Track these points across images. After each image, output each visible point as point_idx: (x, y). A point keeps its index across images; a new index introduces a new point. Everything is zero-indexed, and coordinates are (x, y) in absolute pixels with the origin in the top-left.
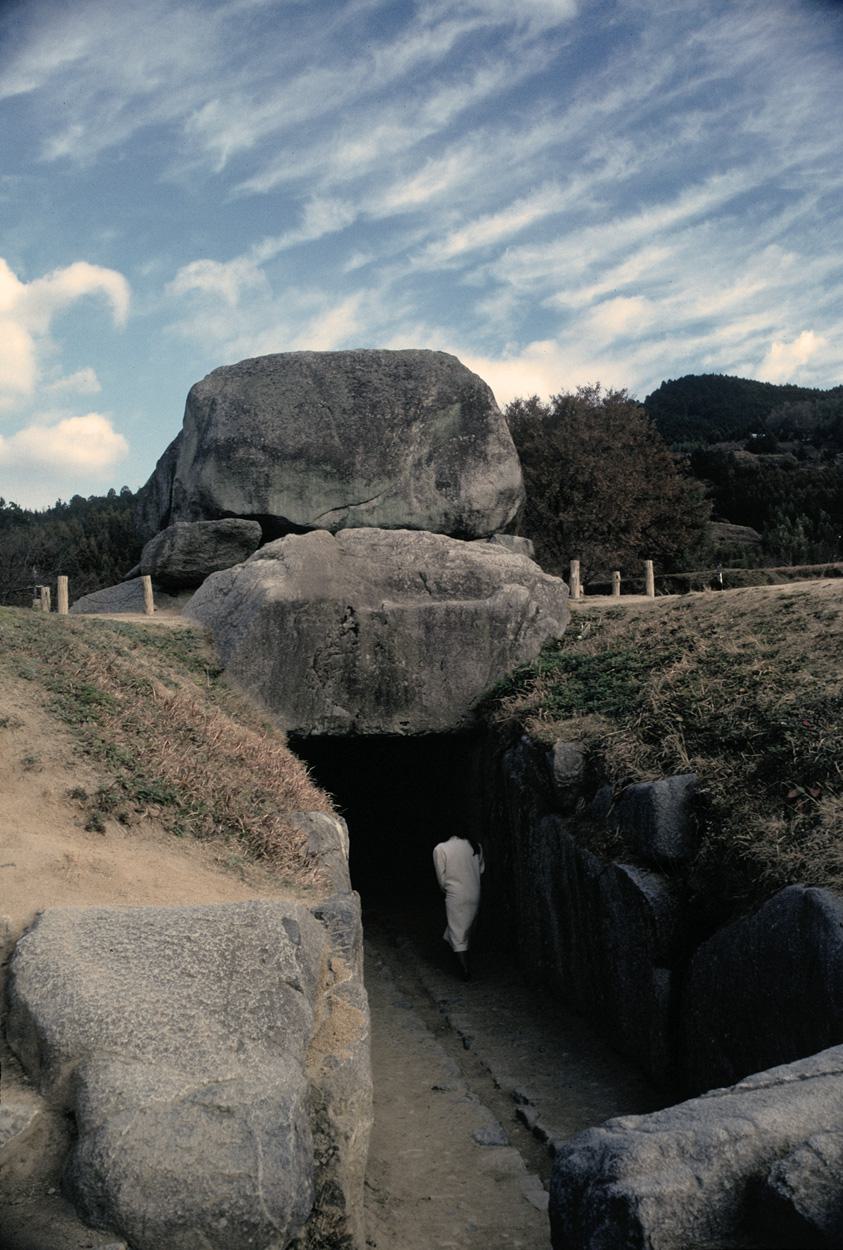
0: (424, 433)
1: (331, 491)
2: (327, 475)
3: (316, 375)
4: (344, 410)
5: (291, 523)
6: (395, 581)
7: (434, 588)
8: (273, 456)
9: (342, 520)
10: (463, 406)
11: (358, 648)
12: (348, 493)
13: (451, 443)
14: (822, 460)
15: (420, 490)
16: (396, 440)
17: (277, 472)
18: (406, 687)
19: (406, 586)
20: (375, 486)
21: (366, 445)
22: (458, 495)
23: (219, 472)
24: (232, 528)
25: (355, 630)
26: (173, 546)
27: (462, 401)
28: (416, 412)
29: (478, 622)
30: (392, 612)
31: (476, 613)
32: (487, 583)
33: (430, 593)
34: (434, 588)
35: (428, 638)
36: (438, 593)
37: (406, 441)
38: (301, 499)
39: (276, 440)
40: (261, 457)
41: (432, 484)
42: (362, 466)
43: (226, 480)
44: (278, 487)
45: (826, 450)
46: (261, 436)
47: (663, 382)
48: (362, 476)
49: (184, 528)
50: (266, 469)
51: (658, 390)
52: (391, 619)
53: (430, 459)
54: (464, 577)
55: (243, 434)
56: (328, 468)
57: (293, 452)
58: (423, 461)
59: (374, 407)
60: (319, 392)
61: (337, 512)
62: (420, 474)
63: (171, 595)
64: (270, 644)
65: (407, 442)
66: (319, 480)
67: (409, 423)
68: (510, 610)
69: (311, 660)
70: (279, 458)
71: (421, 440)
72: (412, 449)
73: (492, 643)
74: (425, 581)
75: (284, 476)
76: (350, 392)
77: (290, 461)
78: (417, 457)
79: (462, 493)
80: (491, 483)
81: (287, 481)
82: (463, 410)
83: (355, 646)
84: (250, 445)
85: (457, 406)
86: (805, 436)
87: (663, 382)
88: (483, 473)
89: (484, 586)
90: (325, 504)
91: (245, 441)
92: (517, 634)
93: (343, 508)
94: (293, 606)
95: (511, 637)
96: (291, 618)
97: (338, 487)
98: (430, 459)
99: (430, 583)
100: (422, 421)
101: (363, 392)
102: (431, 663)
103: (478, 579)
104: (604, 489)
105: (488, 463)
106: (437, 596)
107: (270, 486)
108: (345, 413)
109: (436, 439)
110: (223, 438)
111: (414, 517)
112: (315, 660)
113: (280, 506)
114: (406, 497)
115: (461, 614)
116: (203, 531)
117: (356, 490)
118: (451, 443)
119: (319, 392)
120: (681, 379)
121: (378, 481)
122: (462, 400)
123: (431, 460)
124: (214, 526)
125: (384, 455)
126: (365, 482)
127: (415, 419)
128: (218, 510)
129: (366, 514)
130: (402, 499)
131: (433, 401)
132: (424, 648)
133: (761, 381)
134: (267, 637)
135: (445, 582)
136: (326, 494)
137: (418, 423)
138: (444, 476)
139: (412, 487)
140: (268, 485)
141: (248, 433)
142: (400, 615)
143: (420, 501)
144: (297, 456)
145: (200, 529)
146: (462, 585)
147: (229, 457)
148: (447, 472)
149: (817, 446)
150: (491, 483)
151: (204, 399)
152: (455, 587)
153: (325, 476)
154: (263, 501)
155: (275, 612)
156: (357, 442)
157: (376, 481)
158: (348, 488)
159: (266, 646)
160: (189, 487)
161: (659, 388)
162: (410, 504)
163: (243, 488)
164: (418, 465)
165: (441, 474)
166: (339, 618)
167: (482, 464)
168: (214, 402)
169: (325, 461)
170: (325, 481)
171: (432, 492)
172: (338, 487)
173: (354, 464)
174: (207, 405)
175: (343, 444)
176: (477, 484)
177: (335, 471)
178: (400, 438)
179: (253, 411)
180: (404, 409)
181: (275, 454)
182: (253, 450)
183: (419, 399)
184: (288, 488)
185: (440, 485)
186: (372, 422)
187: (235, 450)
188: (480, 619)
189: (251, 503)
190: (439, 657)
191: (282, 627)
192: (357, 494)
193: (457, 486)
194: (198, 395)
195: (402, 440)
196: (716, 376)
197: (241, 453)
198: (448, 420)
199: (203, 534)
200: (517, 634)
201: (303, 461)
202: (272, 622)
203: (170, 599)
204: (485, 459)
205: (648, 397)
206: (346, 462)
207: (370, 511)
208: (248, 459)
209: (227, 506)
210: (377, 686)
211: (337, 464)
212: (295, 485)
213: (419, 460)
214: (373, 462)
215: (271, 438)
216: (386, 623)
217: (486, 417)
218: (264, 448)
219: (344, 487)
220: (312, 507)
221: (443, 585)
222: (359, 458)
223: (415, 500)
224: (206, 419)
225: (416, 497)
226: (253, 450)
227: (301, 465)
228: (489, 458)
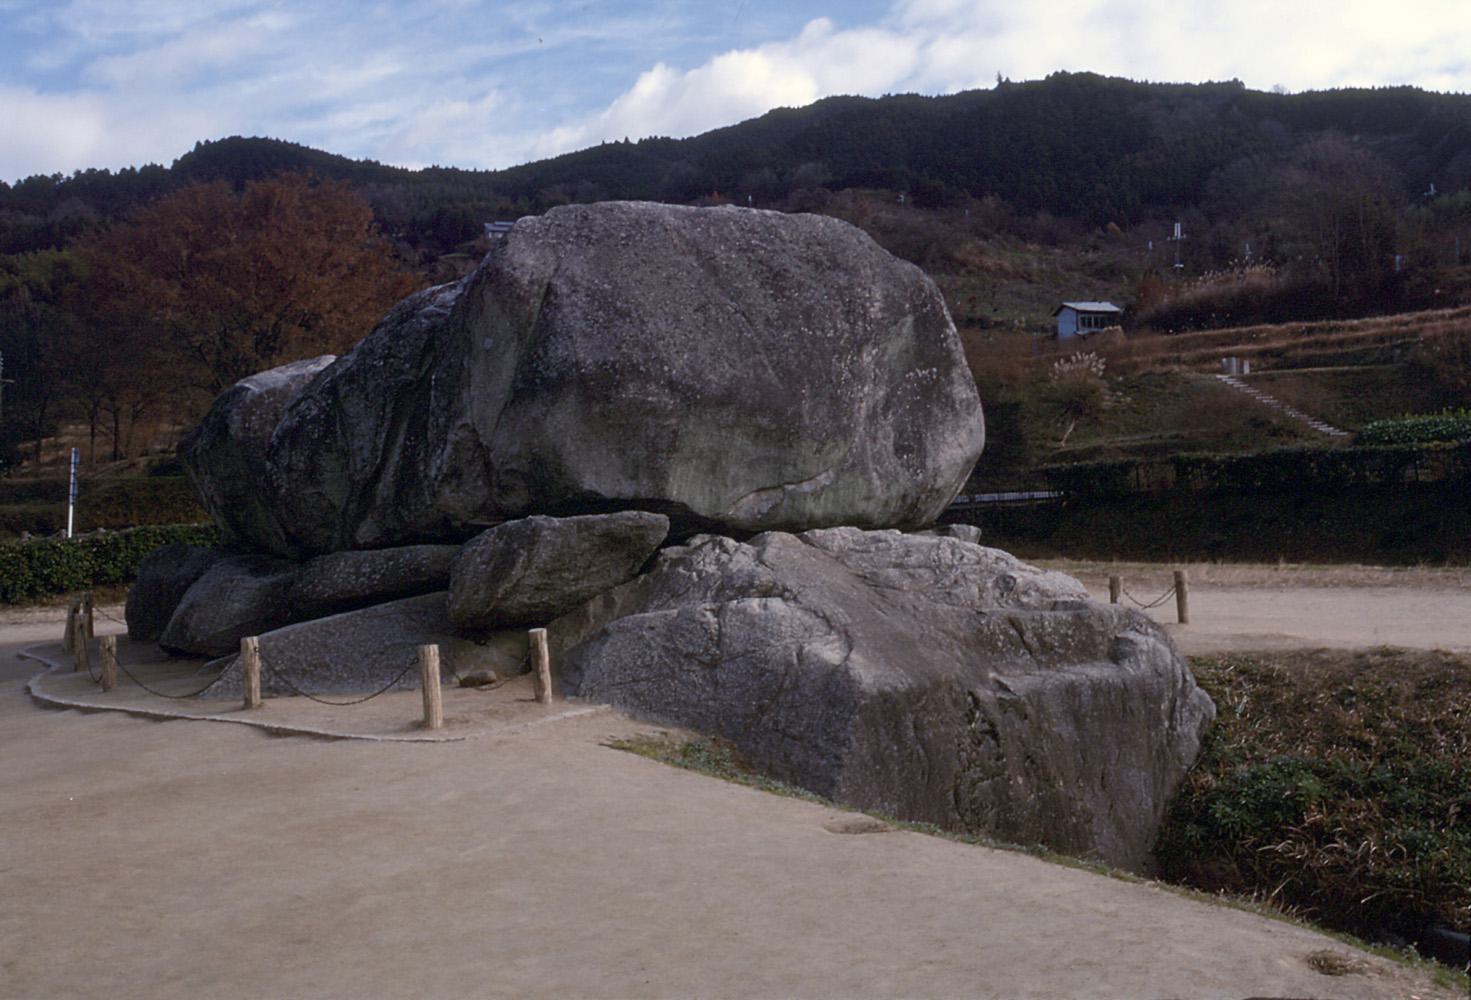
0: (878, 363)
2: (760, 434)
3: (699, 252)
4: (768, 319)
7: (1034, 643)
8: (688, 398)
10: (915, 320)
11: (1005, 767)
12: (786, 464)
13: (908, 381)
14: (421, 263)
15: (878, 459)
16: (846, 374)
19: (1000, 644)
20: (829, 453)
21: (811, 383)
22: (923, 466)
24: (631, 528)
30: (586, 612)
31: (1126, 689)
33: (1031, 653)
34: (1034, 643)
36: (1043, 653)
37: (858, 377)
39: (687, 370)
40: (668, 401)
41: (890, 445)
42: (811, 419)
45: (426, 250)
46: (663, 363)
47: (198, 144)
48: (812, 436)
49: (554, 529)
50: (673, 421)
51: (190, 153)
54: (1071, 624)
56: (765, 422)
58: (879, 410)
59: (808, 314)
61: (764, 496)
62: (876, 431)
63: (478, 643)
65: (860, 379)
66: (746, 442)
67: (858, 346)
68: (1161, 680)
69: (951, 795)
70: (697, 403)
71: (876, 375)
72: (866, 389)
73: (1149, 736)
74: (1021, 633)
76: (762, 285)
78: (871, 404)
79: (929, 463)
81: (702, 442)
82: (917, 323)
83: (1000, 763)
84: (647, 377)
85: (910, 319)
86: (396, 229)
87: (198, 144)
88: (954, 431)
89: (1099, 639)
91: (635, 367)
92: (1171, 718)
95: (1167, 724)
97: (774, 452)
98: (887, 407)
99: (1029, 636)
100: (875, 345)
101: (785, 289)
104: (334, 322)
105: (957, 415)
106: (1044, 659)
107: (676, 451)
109: (892, 373)
112: (956, 794)
113: (685, 486)
114: (865, 471)
115: (1109, 693)
116: (585, 534)
117: (800, 459)
120: (223, 140)
121: (833, 444)
122: (915, 309)
123: (889, 408)
124: (604, 525)
125: (835, 400)
129: (810, 499)
133: (331, 153)
135: (1050, 635)
136: (750, 465)
137: (868, 348)
138: (905, 436)
139: (869, 453)
140: (673, 448)
141: (638, 356)
142: (1036, 695)
143: (880, 477)
145: (580, 531)
146: (1071, 637)
147: (607, 398)
148: (910, 429)
150: (960, 446)
151: (531, 282)
153: (756, 436)
154: (659, 475)
155: (884, 712)
157: (830, 444)
161: (192, 150)
162: (869, 481)
163: (622, 452)
164: (872, 417)
165: (900, 432)
166: (961, 714)
168: (550, 290)
171: (892, 463)
172: (774, 452)
173: (801, 416)
175: (781, 380)
178: (851, 372)
179: (634, 315)
180: (848, 321)
181: (690, 397)
182: (652, 387)
183: (863, 306)
184: (700, 456)
185: (900, 450)
186: (813, 343)
189: (634, 477)
191: (898, 738)
192: (800, 466)
193: (922, 453)
194: (518, 274)
196: (271, 141)
197: (631, 391)
199: (584, 540)
200: (1171, 718)
202: (882, 731)
203: (476, 650)
204: (953, 408)
205: (175, 161)
207: (816, 495)
208: (644, 402)
210: (1042, 830)
213: (874, 408)
214: (823, 411)
215: (679, 365)
216: (1026, 717)
217: (946, 339)
218: (671, 385)
221: (1047, 639)
222: (806, 405)
223: (874, 474)
224: (534, 319)
225: (876, 470)
226: (652, 387)
227: (728, 415)
228: (958, 406)
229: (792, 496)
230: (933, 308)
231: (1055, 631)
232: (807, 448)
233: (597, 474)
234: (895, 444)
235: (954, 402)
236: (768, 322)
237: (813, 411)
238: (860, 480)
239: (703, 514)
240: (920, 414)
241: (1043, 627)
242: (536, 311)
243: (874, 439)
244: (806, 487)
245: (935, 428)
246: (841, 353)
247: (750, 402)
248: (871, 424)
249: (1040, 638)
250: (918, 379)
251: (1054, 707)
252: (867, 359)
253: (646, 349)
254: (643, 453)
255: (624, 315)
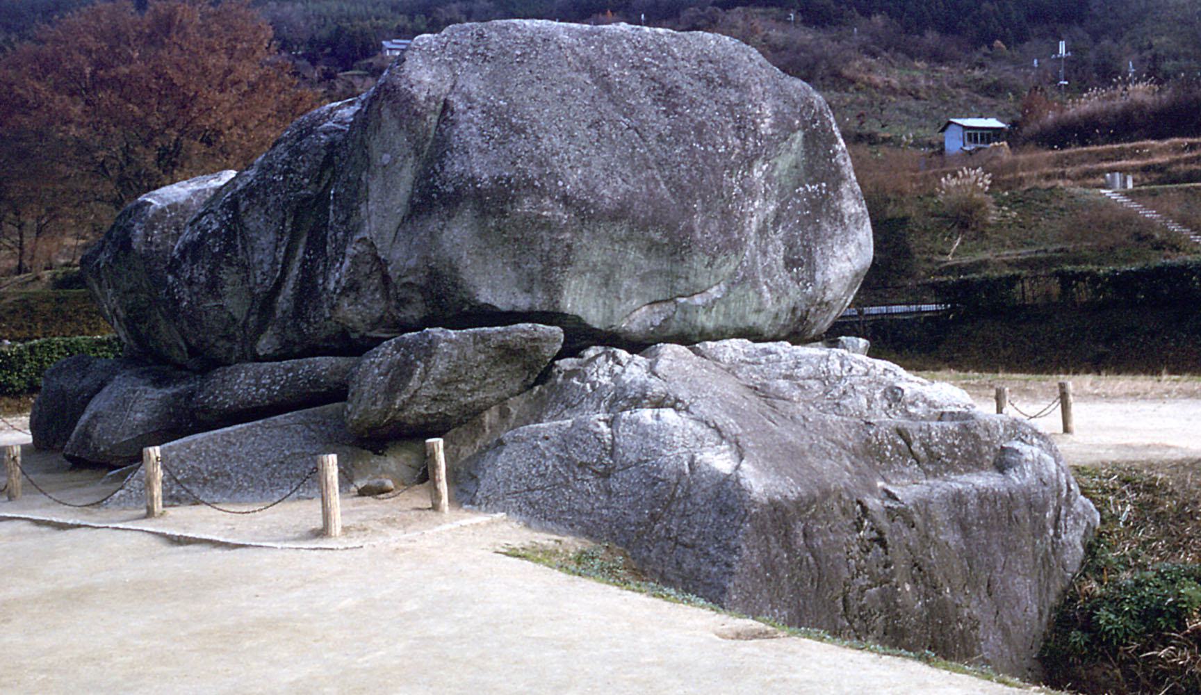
1: (652, 272)
2: (653, 248)
3: (592, 69)
4: (660, 135)
5: (586, 325)
6: (875, 446)
7: (922, 453)
9: (665, 320)
10: (805, 136)
11: (893, 574)
12: (678, 277)
13: (798, 195)
15: (768, 272)
16: (737, 189)
17: (584, 241)
18: (962, 632)
19: (888, 454)
20: (719, 267)
22: (812, 279)
23: (480, 236)
24: (526, 340)
25: (881, 541)
26: (426, 372)
27: (804, 128)
28: (756, 145)
29: (1016, 512)
30: (482, 422)
32: (987, 443)
34: (922, 453)
35: (969, 545)
37: (749, 191)
38: (606, 285)
40: (563, 215)
42: (703, 233)
43: (489, 251)
44: (580, 265)
46: (557, 178)
48: (703, 250)
50: (568, 235)
52: (917, 518)
53: (776, 223)
54: (958, 434)
55: (524, 171)
57: (612, 208)
60: (610, 100)
61: (656, 308)
62: (767, 245)
63: (376, 453)
64: (779, 579)
67: (749, 162)
68: (1046, 489)
70: (591, 218)
71: (766, 191)
75: (593, 249)
77: (609, 224)
80: (849, 259)
81: (596, 256)
83: (888, 570)
84: (541, 192)
85: (799, 135)
88: (842, 246)
90: (639, 294)
91: (530, 183)
93: (666, 301)
94: (798, 509)
95: (1051, 532)
96: (798, 529)
98: (777, 220)
99: (916, 446)
100: (766, 160)
102: (975, 587)
103: (976, 437)
104: (235, 138)
105: (845, 229)
108: (663, 141)
110: (485, 176)
111: (762, 315)
112: (845, 601)
113: (580, 300)
114: (755, 284)
116: (481, 345)
117: (692, 272)
118: (798, 195)
119: (610, 100)
124: (500, 338)
125: (726, 214)
126: (707, 259)
127: (757, 156)
128: (470, 301)
130: (752, 287)
131: (772, 126)
132: (965, 563)
134: (770, 566)
136: (643, 279)
137: (759, 163)
140: (567, 262)
141: (532, 171)
142: (924, 505)
143: (771, 290)
144: (619, 214)
145: (475, 343)
146: (959, 447)
147: (503, 212)
149: (314, 62)
150: (849, 259)
151: (428, 99)
152: (951, 454)
153: (649, 249)
154: (553, 289)
156: (692, 192)
158: (681, 269)
159: (772, 584)
160: (13, 185)
163: (517, 266)
164: (762, 231)
165: (790, 247)
167: (839, 232)
168: (446, 106)
169: (654, 222)
170: (646, 256)
171: (782, 277)
174: (434, 111)
175: (673, 194)
176: (835, 262)
177: (666, 240)
178: (741, 186)
181: (585, 212)
182: (547, 202)
183: (754, 123)
184: (594, 270)
185: (790, 263)
186: (705, 159)
187: (513, 200)
188: (1017, 507)
189: (529, 291)
190: (984, 576)
192: (692, 279)
193: (811, 266)
195: (744, 190)
197: (526, 205)
198: (791, 158)
200: (1056, 527)
201: (625, 223)
203: (374, 460)
206: (683, 224)
207: (708, 308)
208: (539, 216)
209: (485, 296)
211: (670, 229)
212: (604, 262)
214: (714, 226)
215: (572, 180)
218: (566, 200)
219: (675, 268)
220: (619, 299)
221: (934, 449)
222: (698, 220)
225: (766, 283)
226: (547, 202)
227: (621, 229)
228: (846, 221)
229: (685, 309)
230: (822, 124)
231: (942, 441)
232: (698, 262)
233: (493, 287)
234: (785, 258)
235: (843, 216)
236: (660, 138)
237: (705, 224)
238: (751, 293)
239: (597, 326)
240: (810, 228)
241: (930, 437)
242: (432, 127)
243: (765, 253)
244: (698, 300)
245: (825, 243)
246: (732, 168)
247: (643, 216)
248: (761, 238)
249: (927, 447)
250: (808, 194)
251: (941, 516)
252: (757, 174)
253: (540, 165)
254: (538, 267)
255: (520, 131)
